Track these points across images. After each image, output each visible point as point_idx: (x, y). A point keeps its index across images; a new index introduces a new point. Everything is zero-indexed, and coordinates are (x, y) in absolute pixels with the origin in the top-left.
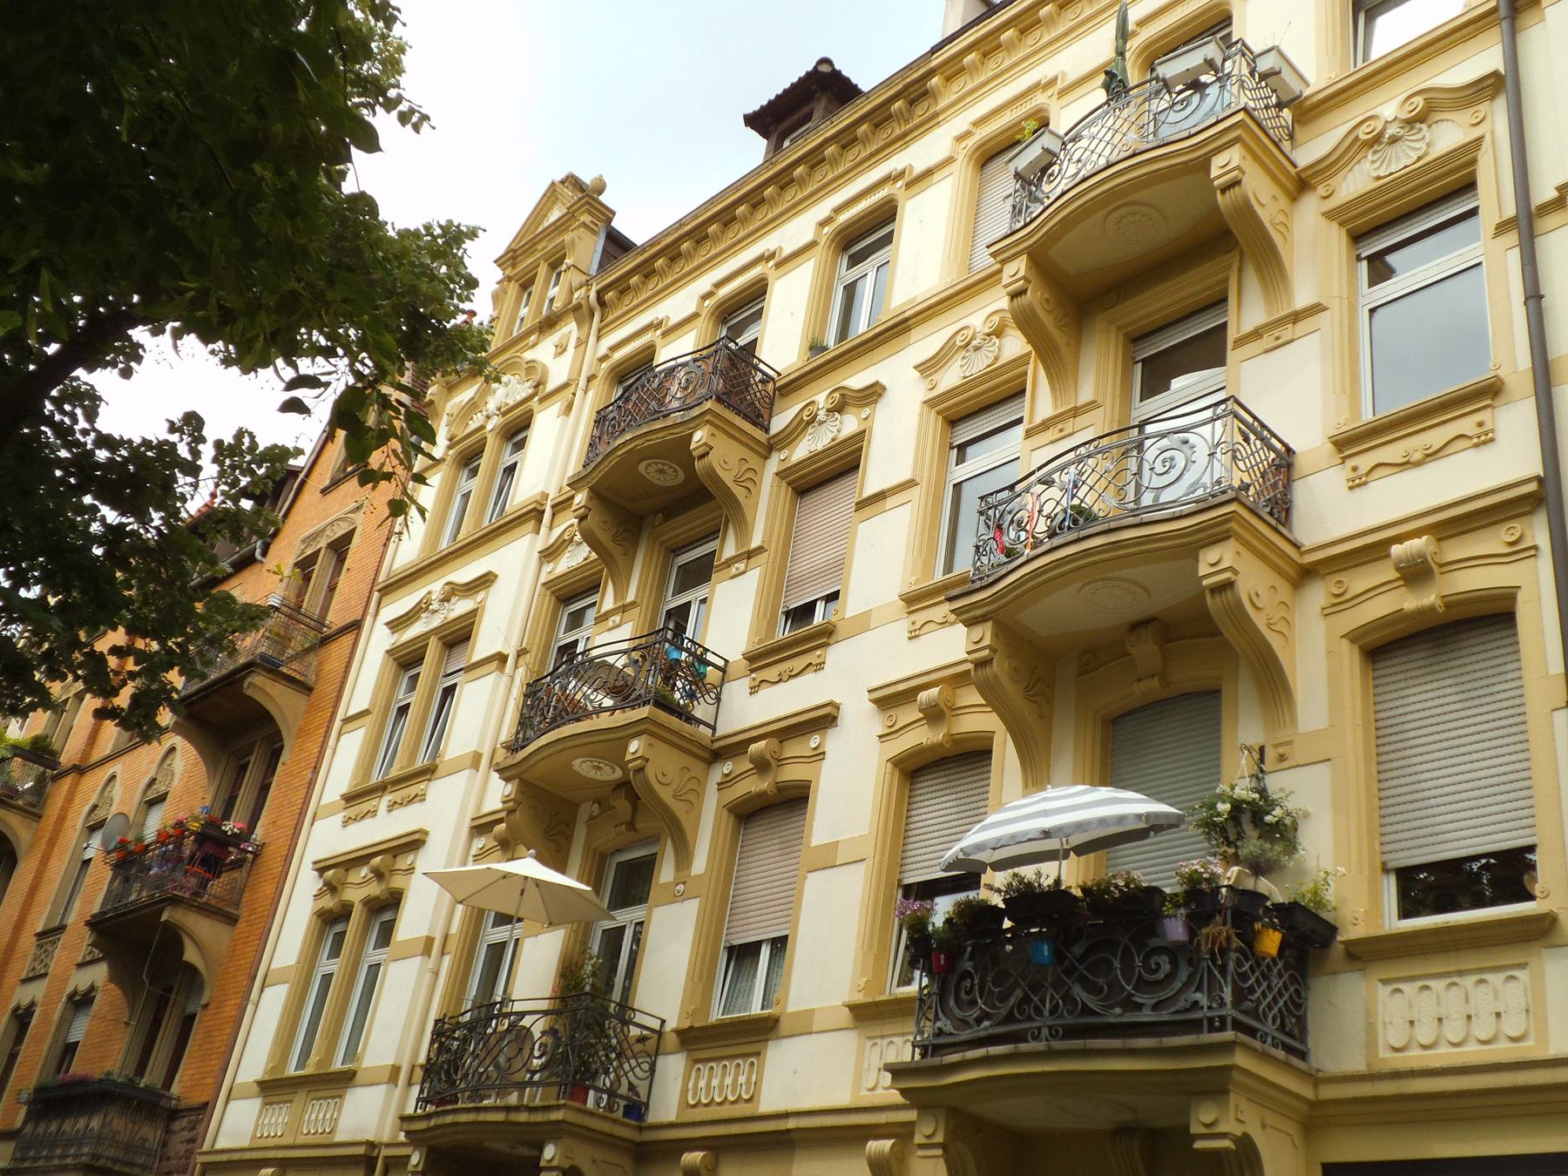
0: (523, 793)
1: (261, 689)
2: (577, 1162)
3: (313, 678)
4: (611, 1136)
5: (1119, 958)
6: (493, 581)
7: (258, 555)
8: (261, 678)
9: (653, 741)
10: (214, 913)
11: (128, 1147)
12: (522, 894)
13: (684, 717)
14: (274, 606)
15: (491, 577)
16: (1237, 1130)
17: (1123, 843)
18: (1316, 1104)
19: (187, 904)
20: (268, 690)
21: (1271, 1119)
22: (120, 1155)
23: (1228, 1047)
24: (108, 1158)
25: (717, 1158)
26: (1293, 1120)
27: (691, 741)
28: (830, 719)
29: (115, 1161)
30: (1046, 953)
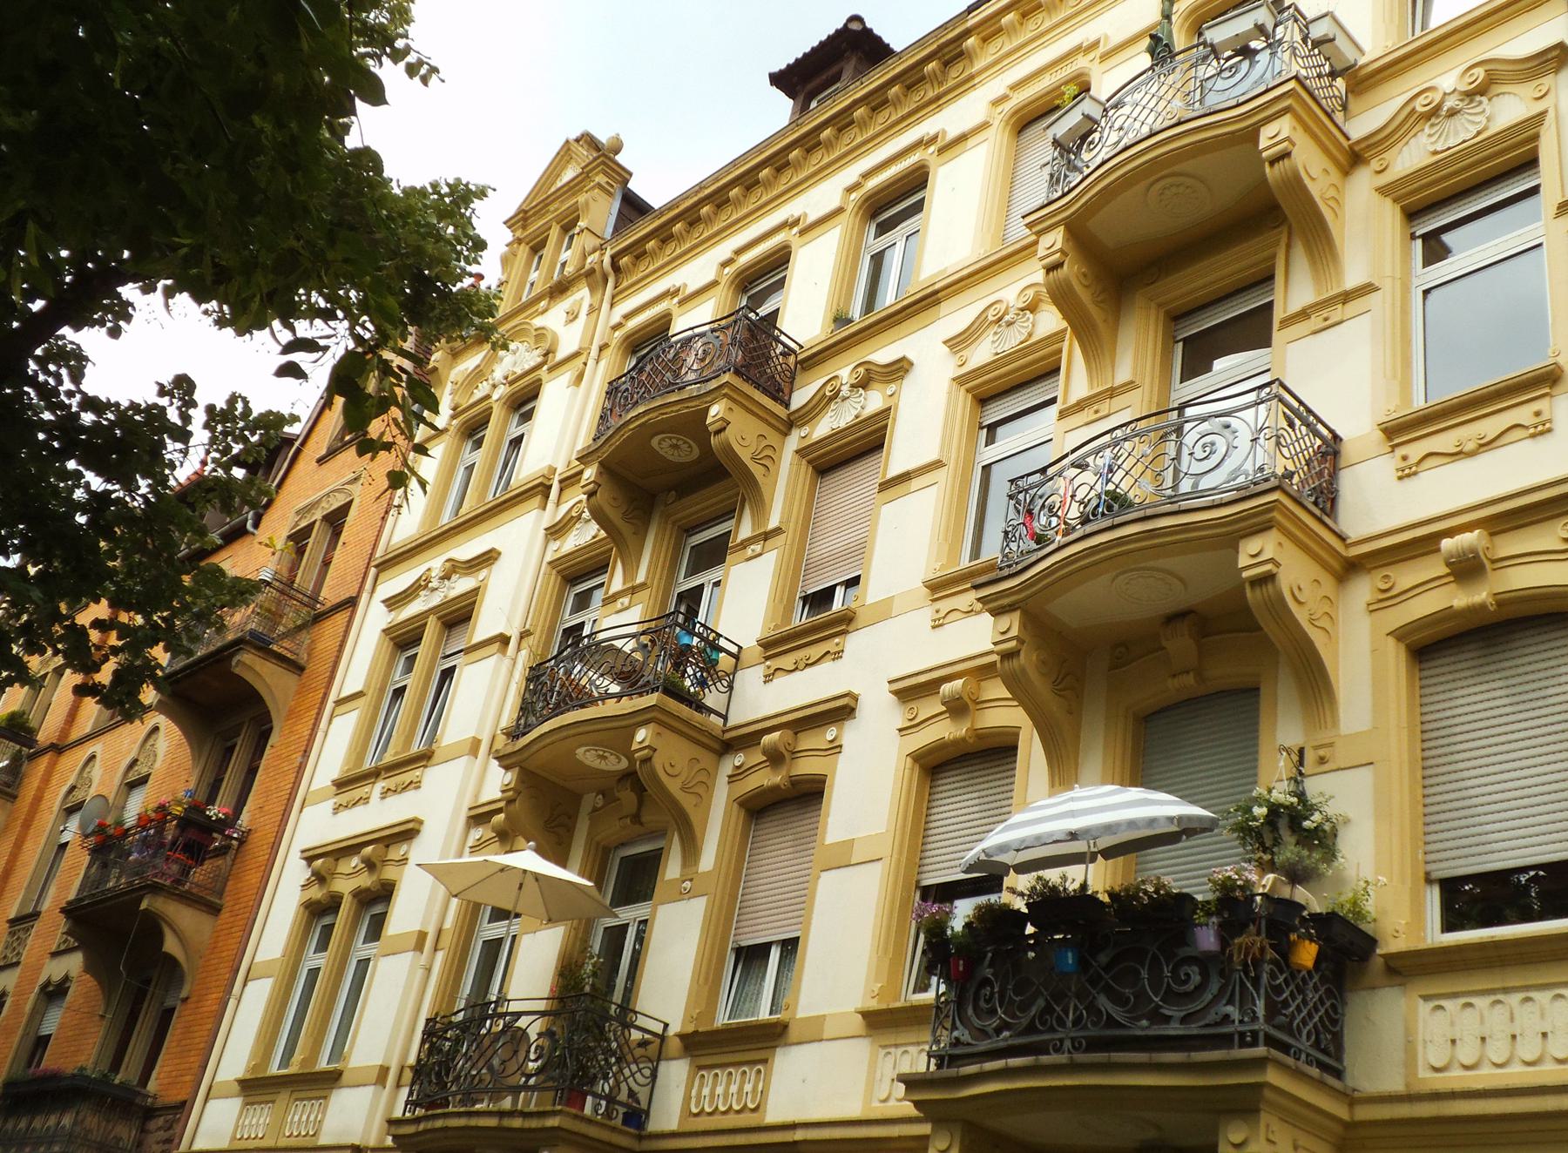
0: (523, 782)
1: (250, 668)
5: (1146, 967)
7: (249, 526)
8: (251, 656)
10: (196, 902)
15: (494, 554)
17: (1153, 847)
19: (169, 892)
20: (258, 668)
23: (1259, 1064)
26: (1330, 1142)
30: (1070, 962)
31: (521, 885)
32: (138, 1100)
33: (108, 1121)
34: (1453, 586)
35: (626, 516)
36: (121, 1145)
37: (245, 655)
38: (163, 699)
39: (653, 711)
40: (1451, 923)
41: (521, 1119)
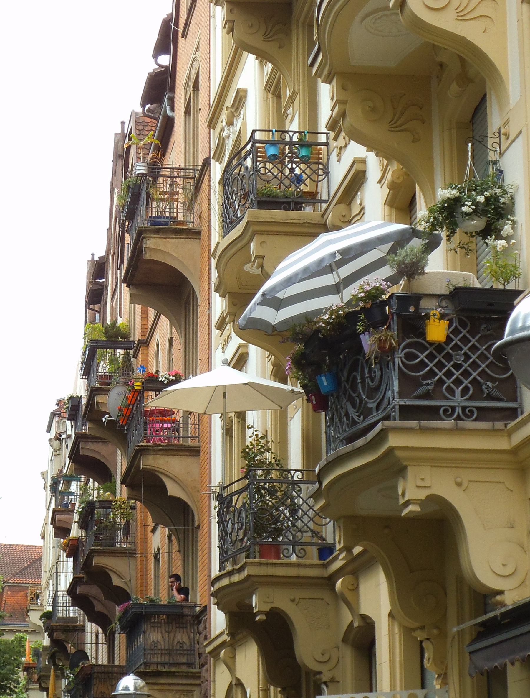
0: (234, 304)
1: (156, 250)
2: (276, 605)
3: (197, 221)
4: (298, 577)
5: (359, 373)
6: (246, 96)
7: (169, 113)
8: (153, 240)
9: (263, 238)
10: (178, 450)
11: (170, 652)
12: (225, 397)
13: (293, 205)
14: (143, 174)
15: (241, 94)
16: (422, 495)
17: (244, 311)
18: (515, 451)
19: (155, 451)
20: (162, 248)
21: (465, 476)
22: (167, 659)
23: (382, 436)
24: (157, 664)
25: (357, 579)
26: (508, 469)
27: (301, 225)
28: (360, 174)
29: (163, 664)
30: (325, 383)
31: (225, 397)
32: (186, 611)
33: (169, 632)
34: (119, 131)
35: (267, 37)
36: (159, 647)
37: (148, 242)
38: (134, 292)
39: (249, 227)
40: (100, 385)
41: (238, 574)
